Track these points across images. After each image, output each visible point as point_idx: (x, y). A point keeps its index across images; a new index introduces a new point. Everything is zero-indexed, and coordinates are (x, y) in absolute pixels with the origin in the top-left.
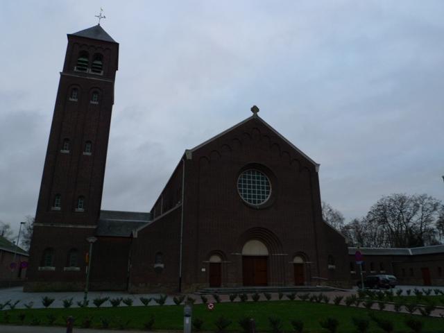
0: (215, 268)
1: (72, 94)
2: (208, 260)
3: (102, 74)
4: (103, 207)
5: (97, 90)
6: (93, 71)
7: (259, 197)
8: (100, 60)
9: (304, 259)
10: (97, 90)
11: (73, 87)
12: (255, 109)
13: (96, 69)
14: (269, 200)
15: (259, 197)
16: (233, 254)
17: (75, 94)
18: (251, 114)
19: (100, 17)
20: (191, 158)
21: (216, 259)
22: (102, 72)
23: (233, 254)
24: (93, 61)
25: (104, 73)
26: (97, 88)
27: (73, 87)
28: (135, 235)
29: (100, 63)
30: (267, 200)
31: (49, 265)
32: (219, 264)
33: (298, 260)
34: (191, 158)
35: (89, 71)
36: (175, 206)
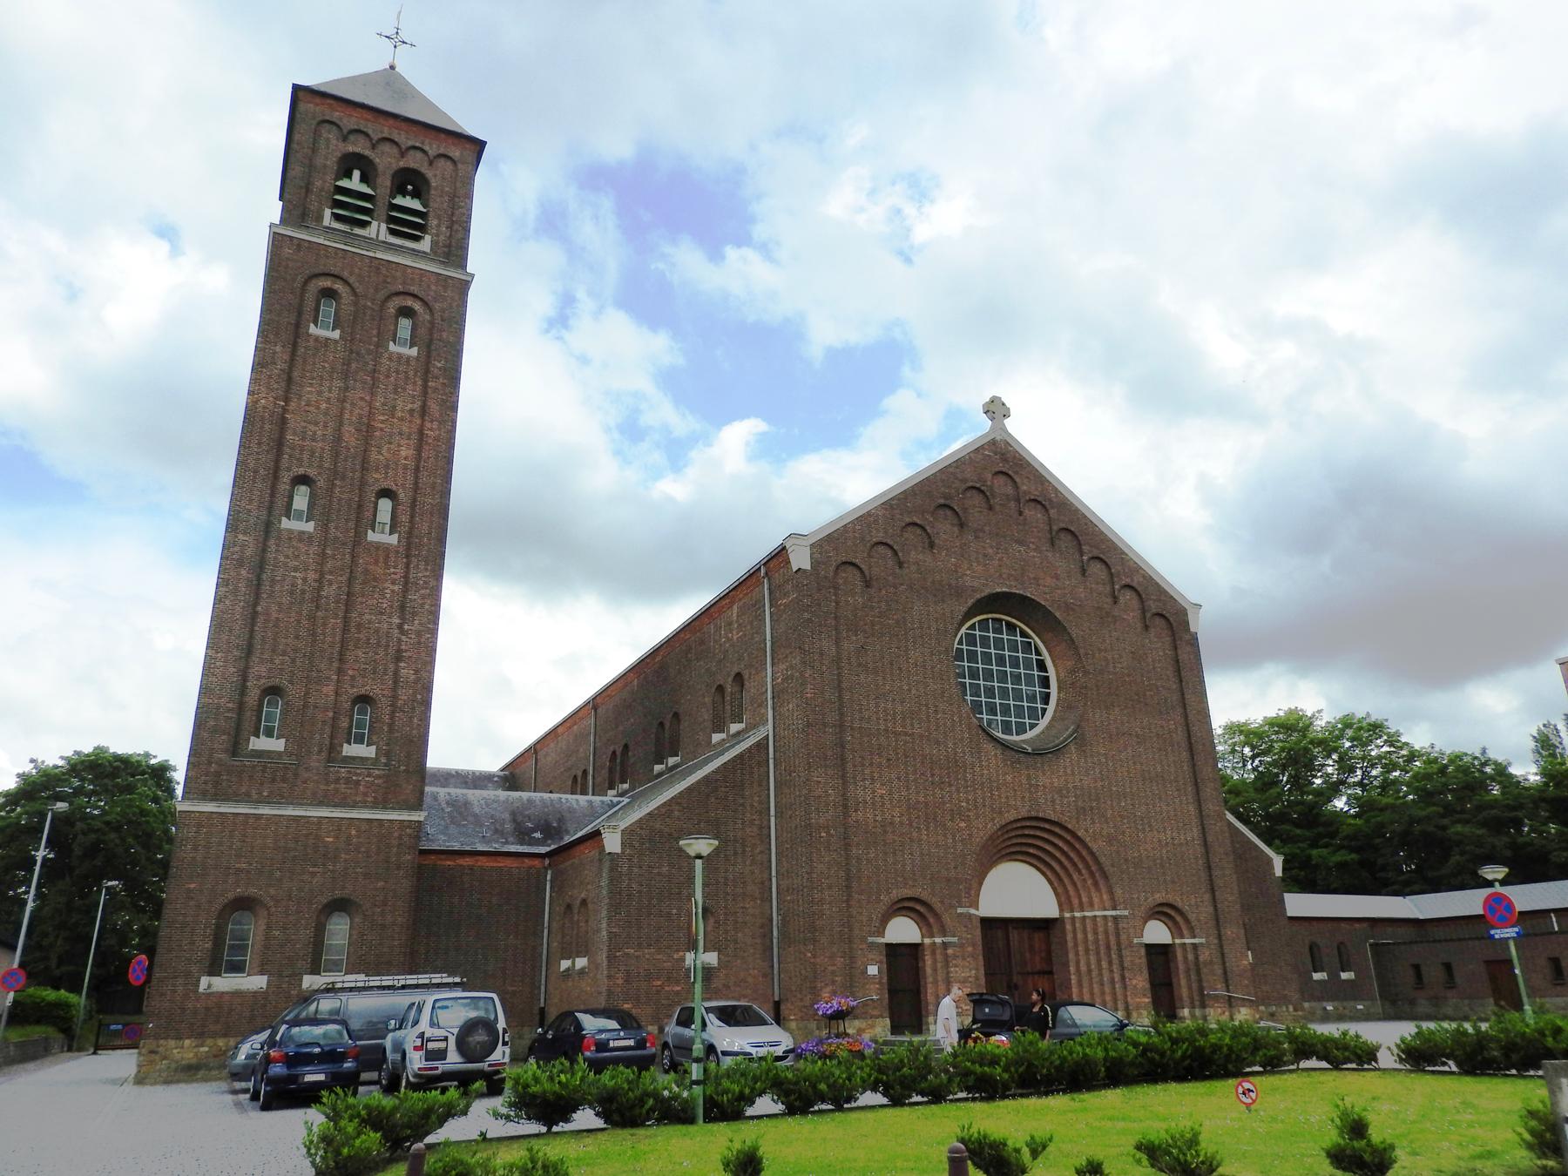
0: (903, 959)
1: (317, 310)
2: (882, 934)
3: (425, 245)
4: (437, 758)
5: (417, 306)
6: (393, 232)
7: (1019, 711)
8: (416, 194)
9: (1176, 930)
10: (417, 306)
11: (326, 283)
12: (996, 409)
13: (407, 227)
14: (1048, 728)
15: (1019, 711)
16: (960, 910)
17: (328, 310)
18: (985, 425)
19: (396, 39)
20: (807, 566)
21: (903, 930)
22: (428, 238)
23: (960, 910)
24: (337, 179)
25: (434, 244)
26: (346, 282)
27: (326, 283)
28: (612, 843)
29: (415, 204)
30: (1043, 723)
31: (237, 968)
32: (914, 949)
33: (1157, 933)
34: (807, 566)
35: (377, 229)
36: (703, 749)
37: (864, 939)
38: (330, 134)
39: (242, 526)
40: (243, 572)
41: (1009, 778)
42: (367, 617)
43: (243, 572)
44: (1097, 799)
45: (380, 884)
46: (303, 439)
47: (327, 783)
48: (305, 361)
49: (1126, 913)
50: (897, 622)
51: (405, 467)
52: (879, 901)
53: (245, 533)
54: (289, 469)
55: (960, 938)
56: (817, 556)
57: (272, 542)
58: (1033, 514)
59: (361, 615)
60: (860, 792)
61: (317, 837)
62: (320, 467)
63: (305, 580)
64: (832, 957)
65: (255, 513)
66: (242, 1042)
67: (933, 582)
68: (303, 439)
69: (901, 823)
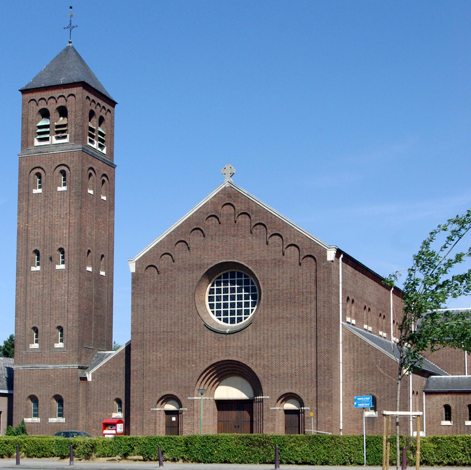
16: (189, 398)
23: (189, 398)
37: (150, 409)
38: (33, 104)
39: (20, 273)
40: (22, 289)
41: (216, 345)
42: (58, 298)
43: (22, 289)
44: (260, 349)
45: (67, 390)
46: (35, 236)
47: (50, 358)
48: (33, 205)
49: (268, 397)
50: (171, 286)
51: (66, 237)
52: (156, 395)
53: (21, 275)
54: (31, 249)
55: (188, 408)
56: (138, 265)
57: (29, 277)
58: (243, 219)
59: (56, 297)
60: (151, 357)
61: (49, 375)
62: (40, 245)
63: (39, 288)
64: (137, 415)
65: (23, 268)
66: (387, 439)
67: (189, 265)
68: (35, 236)
69: (167, 367)
